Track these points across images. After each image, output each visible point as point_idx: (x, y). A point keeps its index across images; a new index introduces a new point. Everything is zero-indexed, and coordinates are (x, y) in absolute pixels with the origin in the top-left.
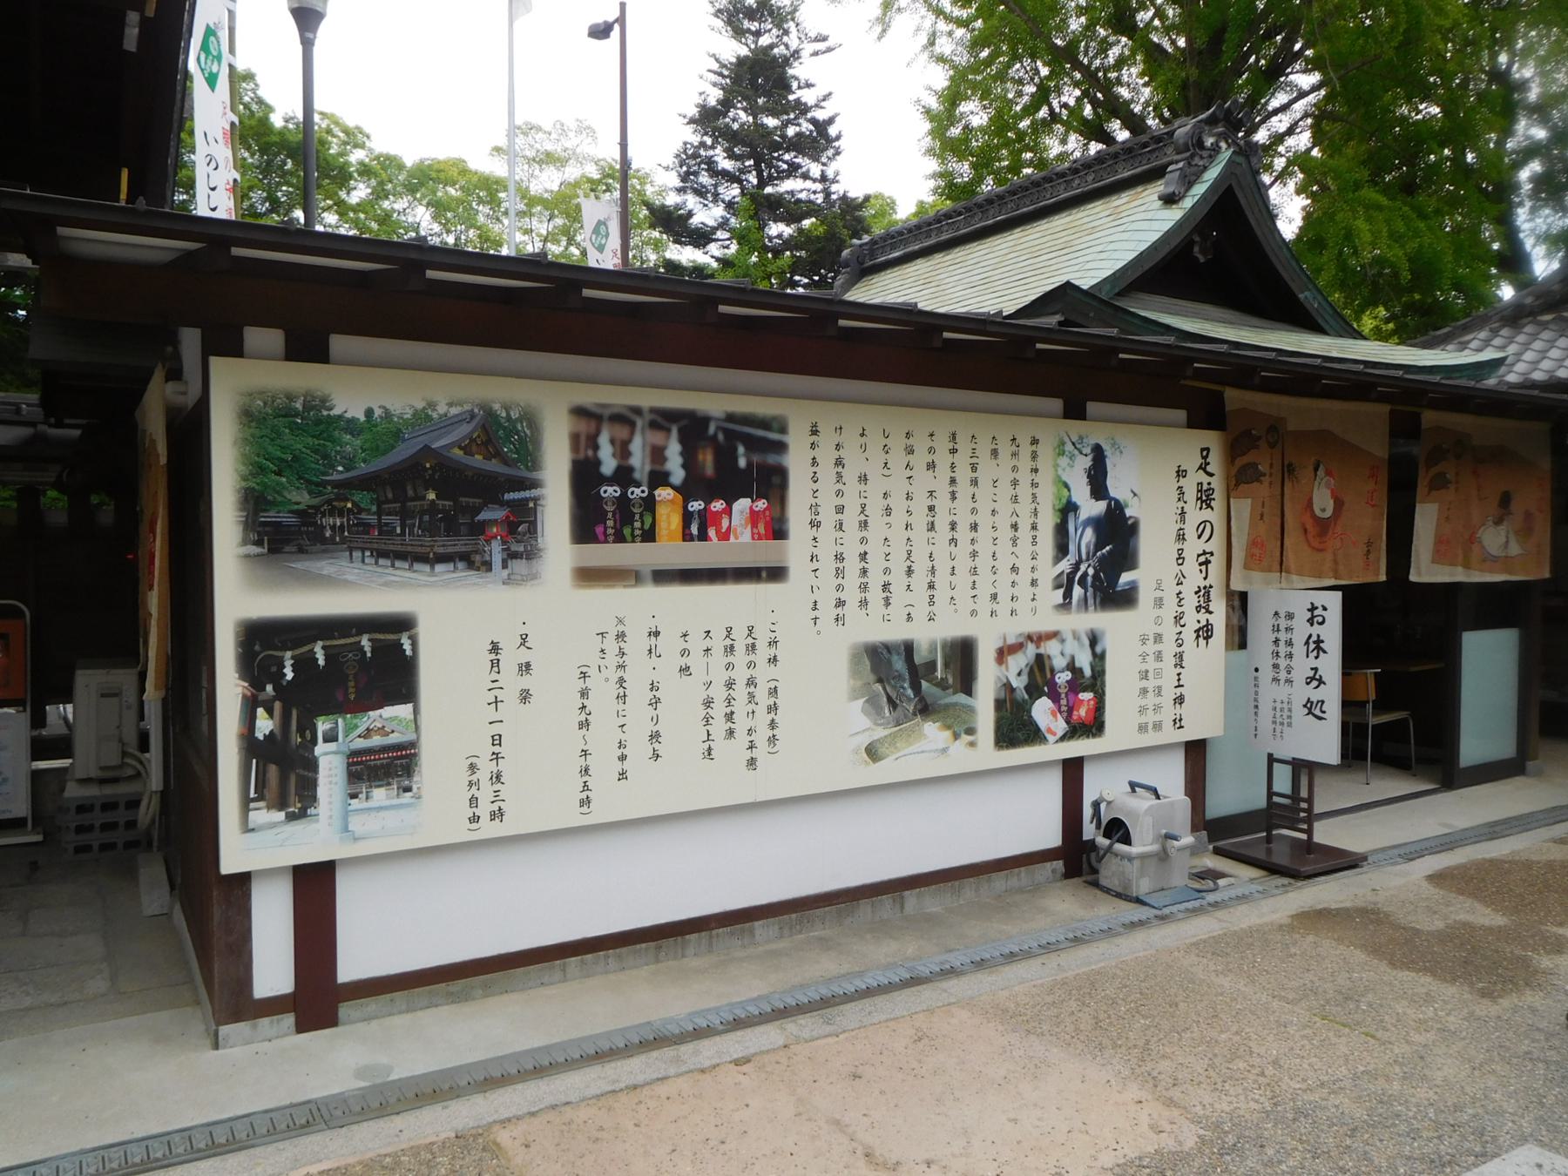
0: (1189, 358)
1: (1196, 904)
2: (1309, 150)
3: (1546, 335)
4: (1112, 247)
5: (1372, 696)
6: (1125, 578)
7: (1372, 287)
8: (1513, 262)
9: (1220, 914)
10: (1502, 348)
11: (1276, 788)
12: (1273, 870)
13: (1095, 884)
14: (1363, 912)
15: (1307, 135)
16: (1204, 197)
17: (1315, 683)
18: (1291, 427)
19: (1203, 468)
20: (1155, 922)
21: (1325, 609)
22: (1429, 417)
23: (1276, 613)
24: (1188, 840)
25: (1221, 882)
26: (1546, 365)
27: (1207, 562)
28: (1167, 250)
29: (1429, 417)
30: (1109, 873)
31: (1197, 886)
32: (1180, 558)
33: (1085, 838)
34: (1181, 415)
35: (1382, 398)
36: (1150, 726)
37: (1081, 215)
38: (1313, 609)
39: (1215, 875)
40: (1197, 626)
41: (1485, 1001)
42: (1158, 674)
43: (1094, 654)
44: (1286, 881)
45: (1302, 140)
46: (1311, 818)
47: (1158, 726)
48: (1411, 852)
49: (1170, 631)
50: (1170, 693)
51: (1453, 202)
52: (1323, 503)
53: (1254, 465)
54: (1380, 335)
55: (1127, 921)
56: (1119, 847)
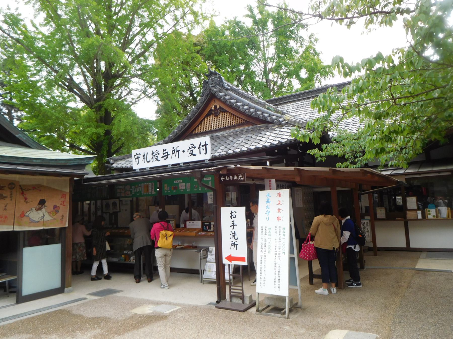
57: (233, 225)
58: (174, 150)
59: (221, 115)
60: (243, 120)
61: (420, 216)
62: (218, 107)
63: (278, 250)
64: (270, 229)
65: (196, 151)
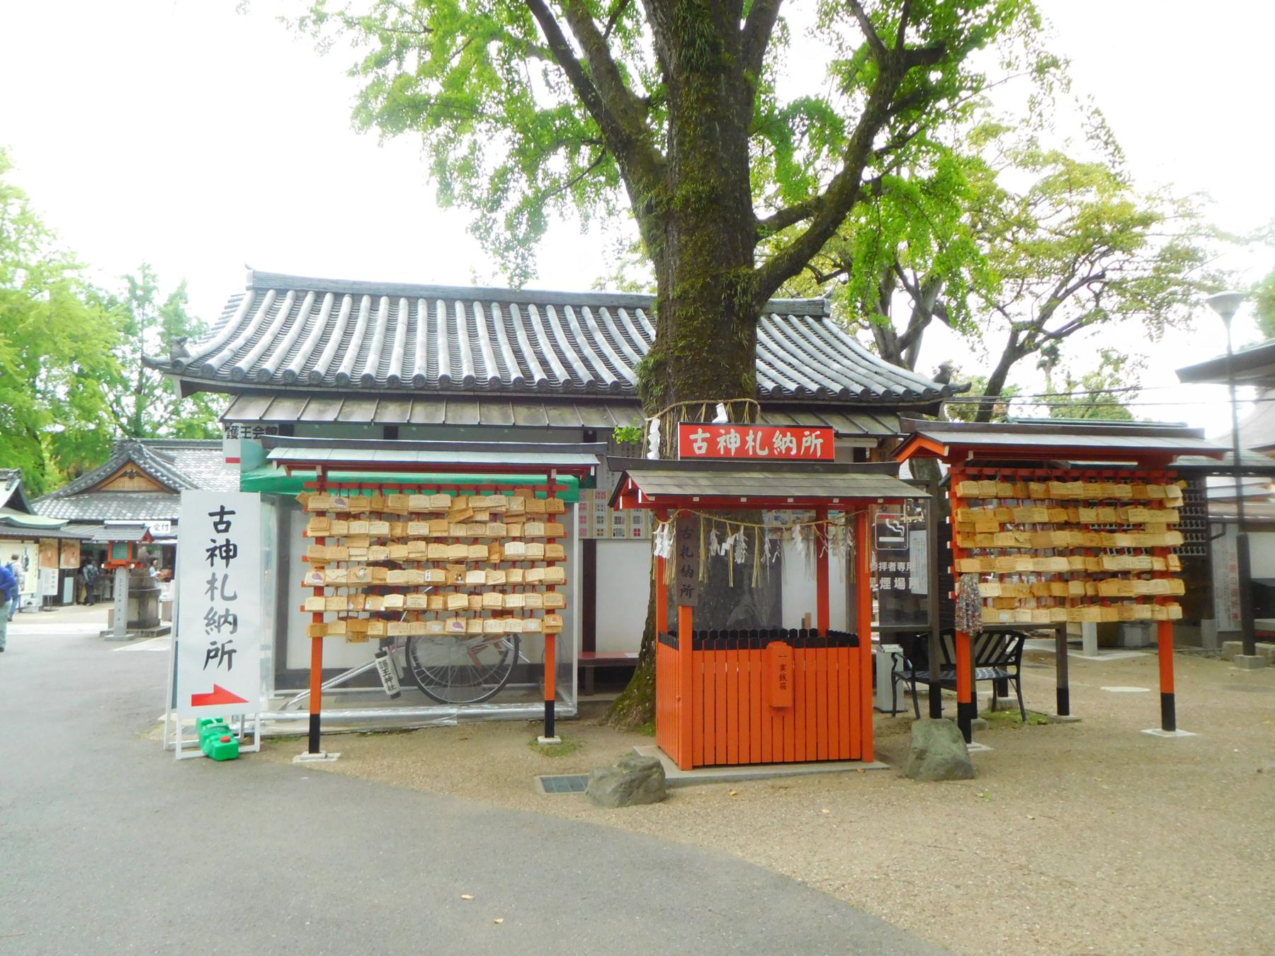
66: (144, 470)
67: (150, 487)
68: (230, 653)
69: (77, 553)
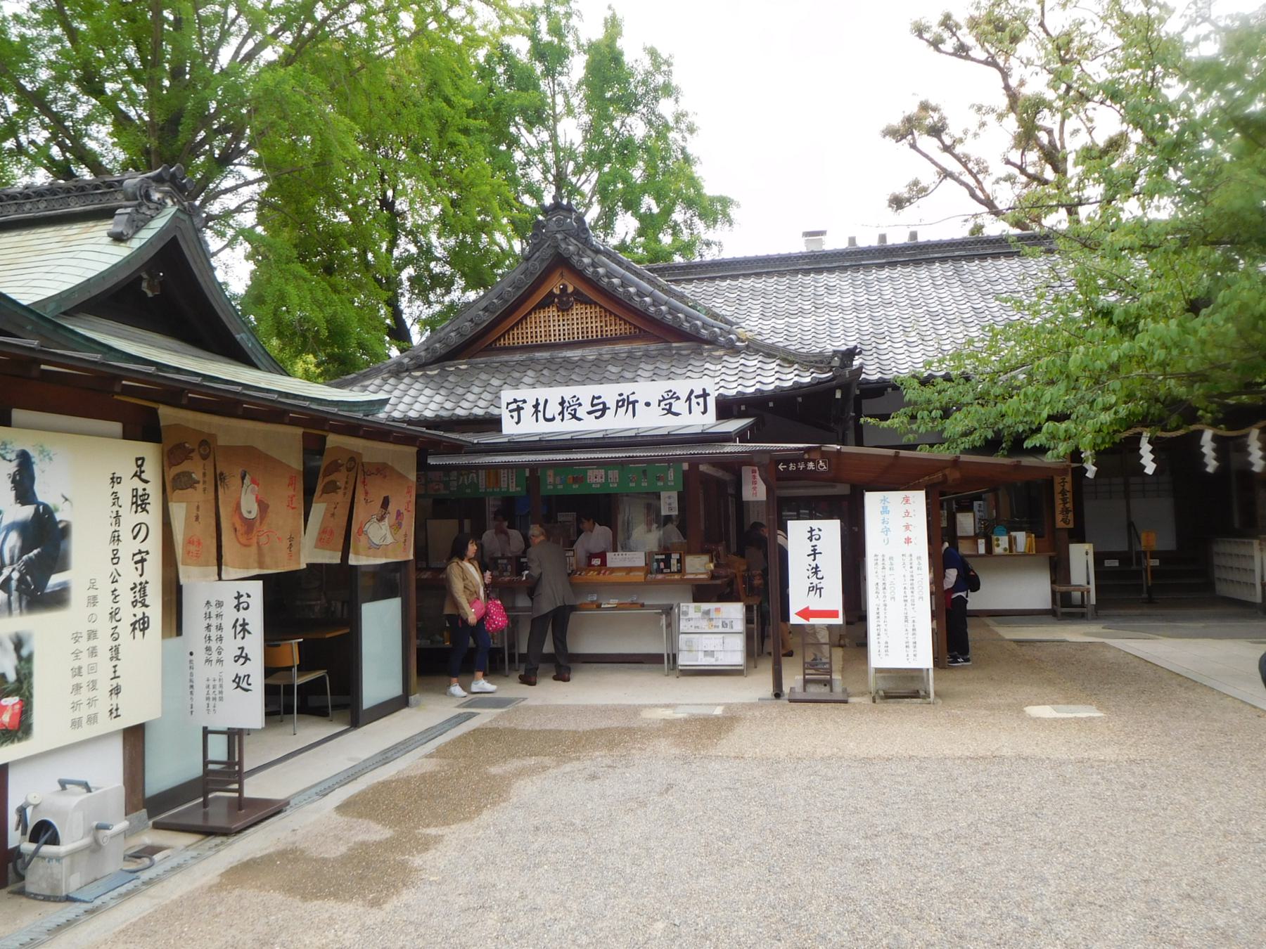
0: (115, 377)
1: (130, 886)
2: (253, 227)
3: (417, 386)
4: (60, 269)
5: (297, 662)
6: (55, 580)
7: (300, 338)
8: (399, 333)
9: (153, 891)
10: (390, 392)
11: (211, 757)
12: (208, 832)
13: (22, 893)
14: (283, 854)
15: (254, 214)
16: (150, 242)
17: (242, 660)
18: (221, 442)
19: (138, 475)
20: (83, 918)
21: (249, 596)
22: (333, 440)
23: (208, 603)
24: (122, 825)
25: (157, 857)
26: (417, 406)
27: (143, 561)
28: (115, 280)
29: (333, 440)
30: (36, 879)
31: (133, 867)
32: (115, 558)
33: (11, 845)
34: (117, 427)
35: (294, 422)
36: (84, 720)
37: (31, 237)
38: (239, 596)
39: (151, 851)
40: (134, 620)
41: (375, 910)
42: (92, 669)
43: (20, 658)
44: (218, 840)
45: (248, 219)
46: (239, 777)
47: (92, 719)
48: (324, 789)
49: (104, 627)
50: (105, 685)
51: (359, 286)
52: (249, 507)
53: (188, 474)
54: (308, 376)
55: (52, 925)
56: (47, 849)
57: (815, 553)
58: (623, 400)
59: (577, 310)
60: (635, 327)
61: (982, 550)
62: (570, 289)
63: (909, 594)
64: (891, 558)
65: (679, 406)
66: (593, 283)
67: (615, 328)
68: (634, 403)
69: (404, 502)
